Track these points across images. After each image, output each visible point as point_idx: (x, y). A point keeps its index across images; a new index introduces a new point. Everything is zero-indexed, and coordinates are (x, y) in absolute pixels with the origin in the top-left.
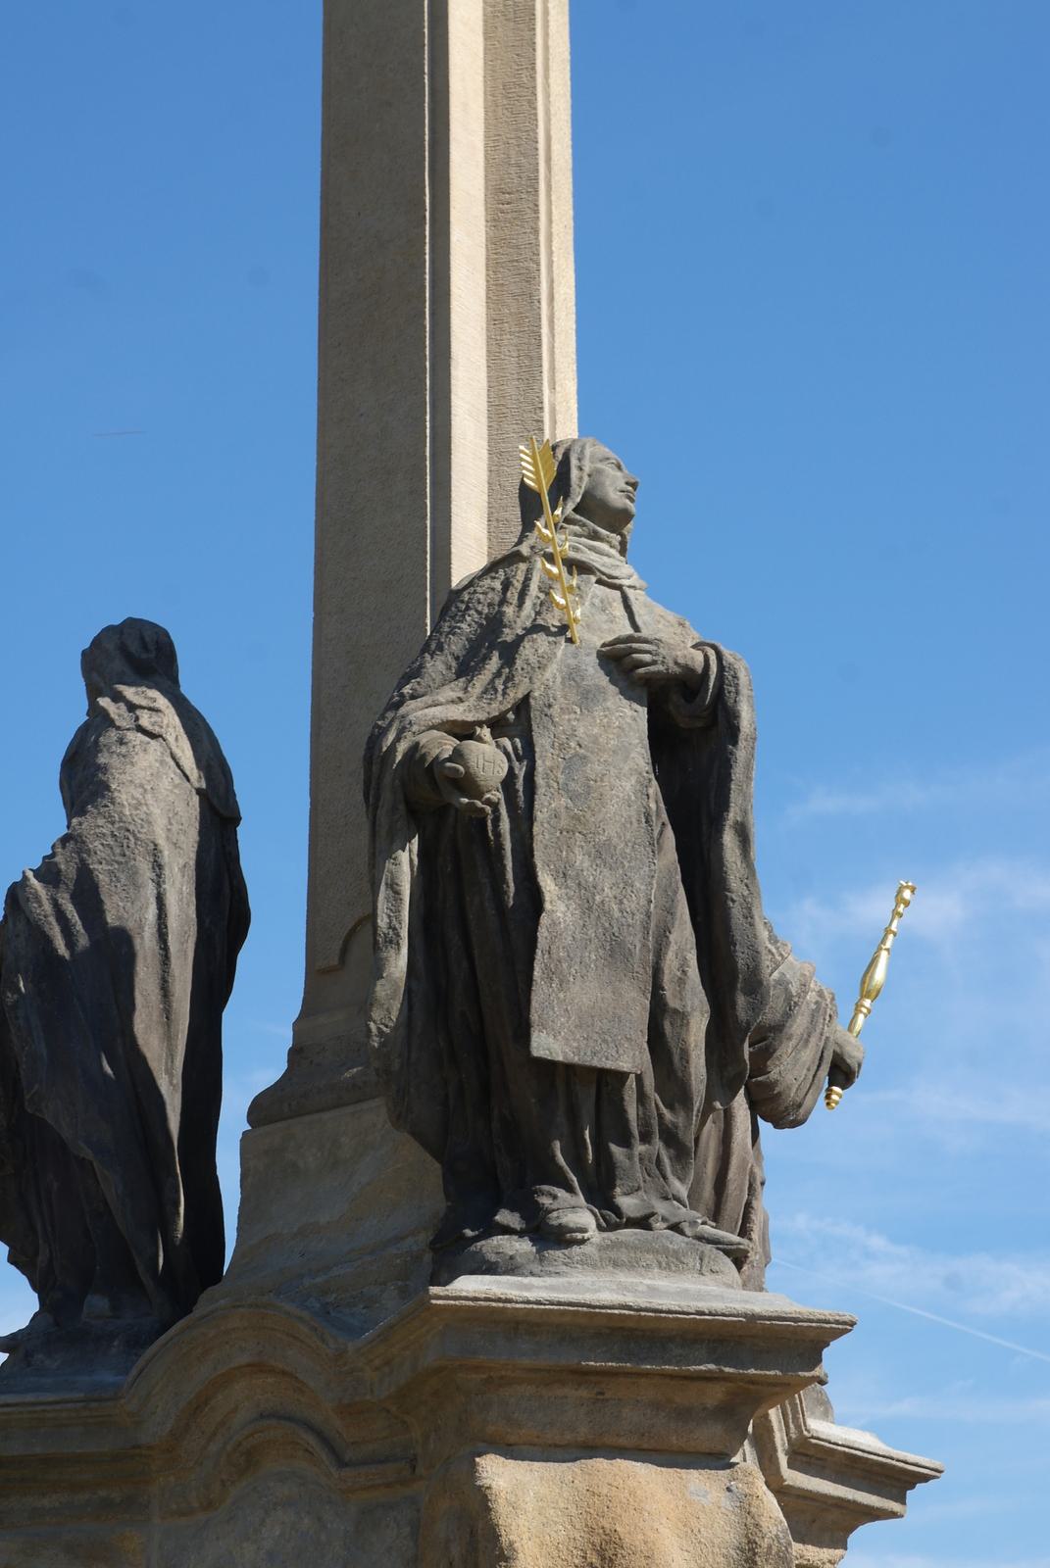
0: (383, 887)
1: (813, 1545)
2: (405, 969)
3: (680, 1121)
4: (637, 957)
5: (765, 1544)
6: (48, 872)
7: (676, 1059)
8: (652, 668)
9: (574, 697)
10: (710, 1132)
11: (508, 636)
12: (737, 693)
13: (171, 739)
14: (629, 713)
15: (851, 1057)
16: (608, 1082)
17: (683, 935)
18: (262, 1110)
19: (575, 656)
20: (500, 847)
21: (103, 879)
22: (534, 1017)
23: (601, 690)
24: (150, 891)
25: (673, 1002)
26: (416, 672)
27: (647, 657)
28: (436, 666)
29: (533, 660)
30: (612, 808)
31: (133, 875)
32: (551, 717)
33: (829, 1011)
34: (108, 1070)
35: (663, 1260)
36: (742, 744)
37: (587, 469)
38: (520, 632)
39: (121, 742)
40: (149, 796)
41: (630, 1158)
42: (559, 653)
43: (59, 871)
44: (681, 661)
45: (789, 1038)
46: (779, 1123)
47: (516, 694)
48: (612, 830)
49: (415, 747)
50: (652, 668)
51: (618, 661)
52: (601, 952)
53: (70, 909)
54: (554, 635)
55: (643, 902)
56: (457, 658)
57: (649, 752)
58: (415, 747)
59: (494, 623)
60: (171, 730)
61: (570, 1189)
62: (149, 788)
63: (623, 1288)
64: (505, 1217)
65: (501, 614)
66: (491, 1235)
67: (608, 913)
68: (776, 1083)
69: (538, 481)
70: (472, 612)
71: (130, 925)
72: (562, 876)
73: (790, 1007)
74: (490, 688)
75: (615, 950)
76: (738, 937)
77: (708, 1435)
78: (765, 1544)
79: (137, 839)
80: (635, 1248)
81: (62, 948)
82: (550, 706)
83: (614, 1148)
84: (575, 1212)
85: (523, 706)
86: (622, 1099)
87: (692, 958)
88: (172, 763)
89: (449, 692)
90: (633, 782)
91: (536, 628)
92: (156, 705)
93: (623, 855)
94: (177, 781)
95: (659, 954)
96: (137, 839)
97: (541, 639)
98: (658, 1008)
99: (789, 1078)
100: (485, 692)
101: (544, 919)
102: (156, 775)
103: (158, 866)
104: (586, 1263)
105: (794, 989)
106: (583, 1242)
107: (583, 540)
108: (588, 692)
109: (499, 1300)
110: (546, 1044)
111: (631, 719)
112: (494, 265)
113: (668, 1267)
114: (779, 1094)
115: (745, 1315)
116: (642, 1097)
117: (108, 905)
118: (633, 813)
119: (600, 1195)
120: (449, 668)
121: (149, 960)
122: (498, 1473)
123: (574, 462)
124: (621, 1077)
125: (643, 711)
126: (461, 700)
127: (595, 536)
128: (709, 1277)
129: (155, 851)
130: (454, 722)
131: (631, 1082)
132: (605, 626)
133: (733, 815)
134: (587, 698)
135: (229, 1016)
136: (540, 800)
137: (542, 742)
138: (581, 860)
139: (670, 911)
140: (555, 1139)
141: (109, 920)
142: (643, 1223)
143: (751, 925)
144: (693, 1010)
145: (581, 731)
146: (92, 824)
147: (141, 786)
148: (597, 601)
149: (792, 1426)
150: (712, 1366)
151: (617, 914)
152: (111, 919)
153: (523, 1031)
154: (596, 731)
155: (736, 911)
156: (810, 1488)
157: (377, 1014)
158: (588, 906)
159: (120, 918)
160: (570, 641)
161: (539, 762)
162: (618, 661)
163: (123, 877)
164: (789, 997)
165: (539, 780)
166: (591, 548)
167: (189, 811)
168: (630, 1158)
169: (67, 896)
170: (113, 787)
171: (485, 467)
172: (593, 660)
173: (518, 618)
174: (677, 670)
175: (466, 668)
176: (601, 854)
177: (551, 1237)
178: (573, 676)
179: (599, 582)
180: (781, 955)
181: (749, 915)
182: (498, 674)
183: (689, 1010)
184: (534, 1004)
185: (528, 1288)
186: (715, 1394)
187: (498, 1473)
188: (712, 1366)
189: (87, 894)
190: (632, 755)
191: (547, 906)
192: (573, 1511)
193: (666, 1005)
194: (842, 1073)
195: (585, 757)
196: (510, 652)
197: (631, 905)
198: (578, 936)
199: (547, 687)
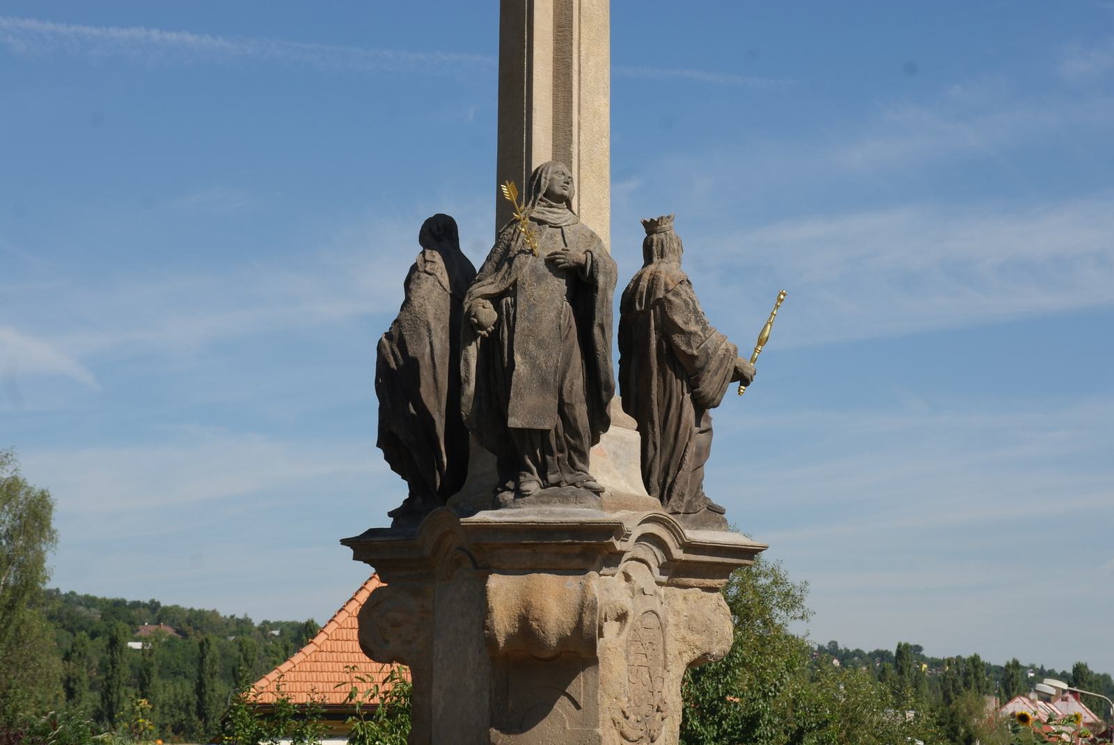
0: (462, 361)
1: (709, 578)
2: (474, 390)
3: (578, 443)
4: (552, 385)
5: (587, 603)
7: (572, 421)
8: (564, 265)
9: (534, 278)
10: (673, 415)
12: (598, 272)
13: (438, 274)
14: (556, 283)
15: (746, 374)
16: (544, 433)
19: (535, 262)
20: (503, 343)
21: (407, 338)
22: (509, 412)
23: (545, 275)
24: (427, 340)
25: (567, 400)
27: (562, 261)
29: (518, 265)
30: (545, 325)
31: (419, 334)
32: (524, 289)
33: (731, 357)
34: (412, 411)
35: (561, 500)
36: (600, 293)
37: (548, 178)
38: (516, 252)
39: (419, 278)
40: (426, 302)
41: (553, 460)
42: (529, 261)
43: (392, 335)
44: (575, 261)
45: (709, 371)
47: (511, 280)
48: (544, 334)
50: (564, 265)
51: (551, 263)
52: (538, 384)
53: (396, 350)
54: (528, 253)
55: (556, 362)
56: (496, 263)
57: (421, 373)
60: (439, 270)
61: (532, 473)
62: (426, 298)
63: (540, 513)
65: (510, 244)
66: (505, 491)
67: (540, 368)
68: (701, 392)
69: (511, 196)
70: (502, 243)
71: (418, 356)
72: (524, 354)
73: (708, 357)
74: (504, 278)
75: (544, 383)
76: (601, 369)
77: (578, 563)
78: (587, 603)
79: (420, 320)
80: (550, 496)
81: (393, 365)
82: (524, 284)
83: (548, 457)
84: (532, 485)
85: (514, 284)
86: (549, 439)
88: (439, 284)
90: (555, 312)
91: (521, 252)
92: (434, 260)
93: (549, 344)
94: (440, 291)
96: (420, 320)
97: (522, 256)
99: (708, 389)
100: (501, 279)
101: (515, 373)
102: (431, 291)
103: (429, 330)
104: (532, 503)
105: (710, 351)
106: (529, 495)
107: (547, 208)
108: (539, 276)
109: (486, 522)
111: (558, 286)
113: (563, 502)
114: (704, 396)
115: (579, 523)
116: (557, 436)
117: (409, 349)
118: (555, 326)
120: (493, 267)
121: (428, 368)
123: (543, 175)
124: (549, 431)
126: (493, 283)
127: (551, 206)
128: (579, 505)
129: (428, 325)
130: (487, 294)
132: (551, 246)
133: (597, 321)
134: (539, 279)
137: (520, 299)
138: (532, 347)
139: (567, 363)
140: (525, 454)
141: (410, 354)
142: (558, 484)
143: (607, 364)
144: (576, 402)
145: (535, 293)
147: (423, 297)
148: (548, 236)
149: (679, 539)
150: (570, 541)
151: (544, 368)
154: (542, 293)
155: (600, 359)
156: (697, 560)
157: (463, 408)
158: (534, 366)
159: (415, 353)
160: (534, 255)
161: (518, 308)
162: (551, 263)
163: (415, 336)
164: (708, 354)
165: (518, 316)
166: (549, 212)
167: (445, 305)
168: (553, 460)
169: (395, 345)
170: (412, 299)
171: (551, 152)
172: (543, 262)
174: (574, 264)
176: (540, 344)
177: (519, 494)
178: (534, 270)
179: (550, 227)
180: (705, 337)
181: (605, 360)
182: (506, 272)
183: (574, 402)
184: (510, 407)
185: (502, 515)
186: (578, 549)
188: (570, 541)
189: (402, 344)
190: (556, 301)
191: (516, 368)
192: (518, 593)
193: (564, 402)
195: (536, 304)
196: (511, 261)
197: (551, 363)
198: (529, 378)
199: (524, 276)
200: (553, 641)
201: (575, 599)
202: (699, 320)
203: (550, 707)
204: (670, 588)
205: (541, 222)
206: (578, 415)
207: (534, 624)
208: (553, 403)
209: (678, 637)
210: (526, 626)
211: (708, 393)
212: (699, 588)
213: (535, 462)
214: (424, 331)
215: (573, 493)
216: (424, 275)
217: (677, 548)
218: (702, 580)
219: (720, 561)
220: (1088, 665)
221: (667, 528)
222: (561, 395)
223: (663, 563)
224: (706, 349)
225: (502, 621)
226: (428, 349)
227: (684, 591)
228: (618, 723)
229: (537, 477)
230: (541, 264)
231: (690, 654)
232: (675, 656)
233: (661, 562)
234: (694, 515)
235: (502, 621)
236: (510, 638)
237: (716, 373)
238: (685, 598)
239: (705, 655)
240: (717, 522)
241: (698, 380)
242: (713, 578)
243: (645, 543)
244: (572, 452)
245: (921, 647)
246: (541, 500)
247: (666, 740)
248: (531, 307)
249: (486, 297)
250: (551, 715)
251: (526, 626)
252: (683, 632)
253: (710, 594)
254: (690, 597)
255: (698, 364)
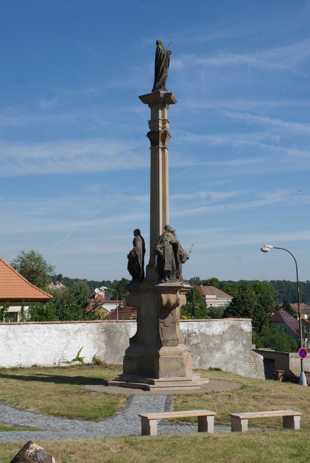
6: (132, 251)
11: (163, 241)
16: (169, 271)
17: (174, 261)
18: (147, 266)
25: (173, 265)
26: (157, 243)
28: (159, 243)
31: (138, 251)
46: (183, 263)
47: (164, 245)
49: (157, 250)
51: (170, 243)
53: (134, 254)
58: (157, 250)
59: (162, 240)
64: (163, 279)
72: (166, 258)
73: (184, 255)
74: (162, 245)
75: (170, 262)
81: (134, 256)
84: (168, 279)
85: (164, 246)
87: (175, 263)
88: (142, 394)
89: (160, 245)
91: (165, 240)
95: (173, 262)
97: (165, 241)
98: (173, 266)
103: (140, 250)
104: (168, 282)
110: (165, 269)
111: (171, 246)
112: (163, 205)
116: (171, 271)
119: (169, 278)
122: (163, 295)
125: (172, 246)
131: (171, 271)
134: (168, 245)
135: (145, 256)
136: (165, 253)
137: (165, 249)
138: (168, 257)
146: (135, 248)
152: (137, 254)
153: (164, 268)
158: (168, 260)
167: (142, 246)
172: (169, 242)
173: (164, 240)
175: (160, 243)
176: (169, 256)
177: (166, 281)
178: (167, 244)
187: (163, 295)
189: (135, 253)
194: (188, 259)
196: (163, 242)
200: (172, 305)
201: (176, 298)
202: (182, 249)
203: (168, 315)
205: (168, 235)
207: (170, 302)
208: (171, 266)
210: (168, 302)
213: (167, 276)
214: (139, 251)
215: (174, 281)
216: (138, 241)
222: (172, 264)
224: (183, 254)
225: (165, 302)
226: (140, 254)
229: (168, 278)
230: (168, 243)
235: (165, 302)
236: (165, 304)
241: (182, 259)
245: (114, 281)
246: (170, 282)
248: (167, 250)
249: (159, 248)
250: (169, 316)
251: (168, 302)
254: (182, 296)
255: (182, 256)
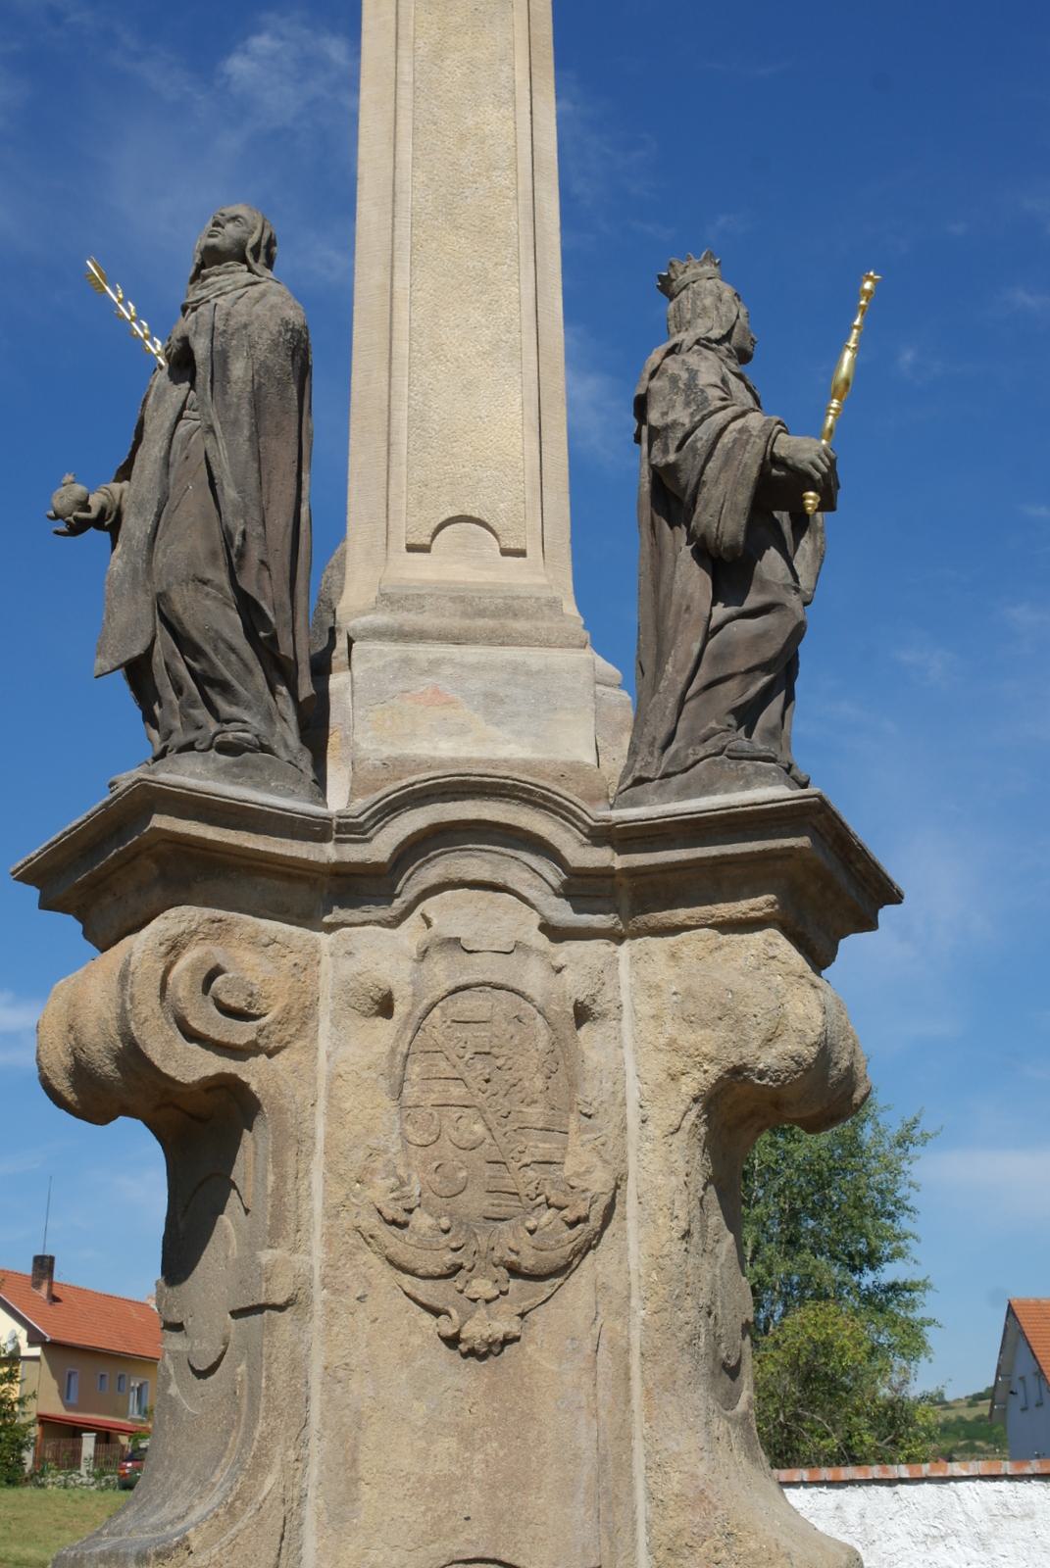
15: (801, 461)
149: (579, 824)
204: (639, 940)
206: (181, 611)
209: (662, 1041)
211: (708, 526)
212: (710, 926)
217: (583, 845)
218: (709, 907)
219: (451, 805)
220: (838, 461)
221: (535, 805)
223: (564, 884)
227: (671, 940)
228: (372, 1237)
231: (698, 1075)
232: (659, 1086)
233: (556, 883)
234: (685, 775)
237: (716, 482)
238: (673, 956)
239: (737, 1071)
240: (739, 778)
242: (735, 898)
243: (470, 846)
244: (207, 689)
247: (640, 1276)
252: (671, 1029)
253: (745, 936)
